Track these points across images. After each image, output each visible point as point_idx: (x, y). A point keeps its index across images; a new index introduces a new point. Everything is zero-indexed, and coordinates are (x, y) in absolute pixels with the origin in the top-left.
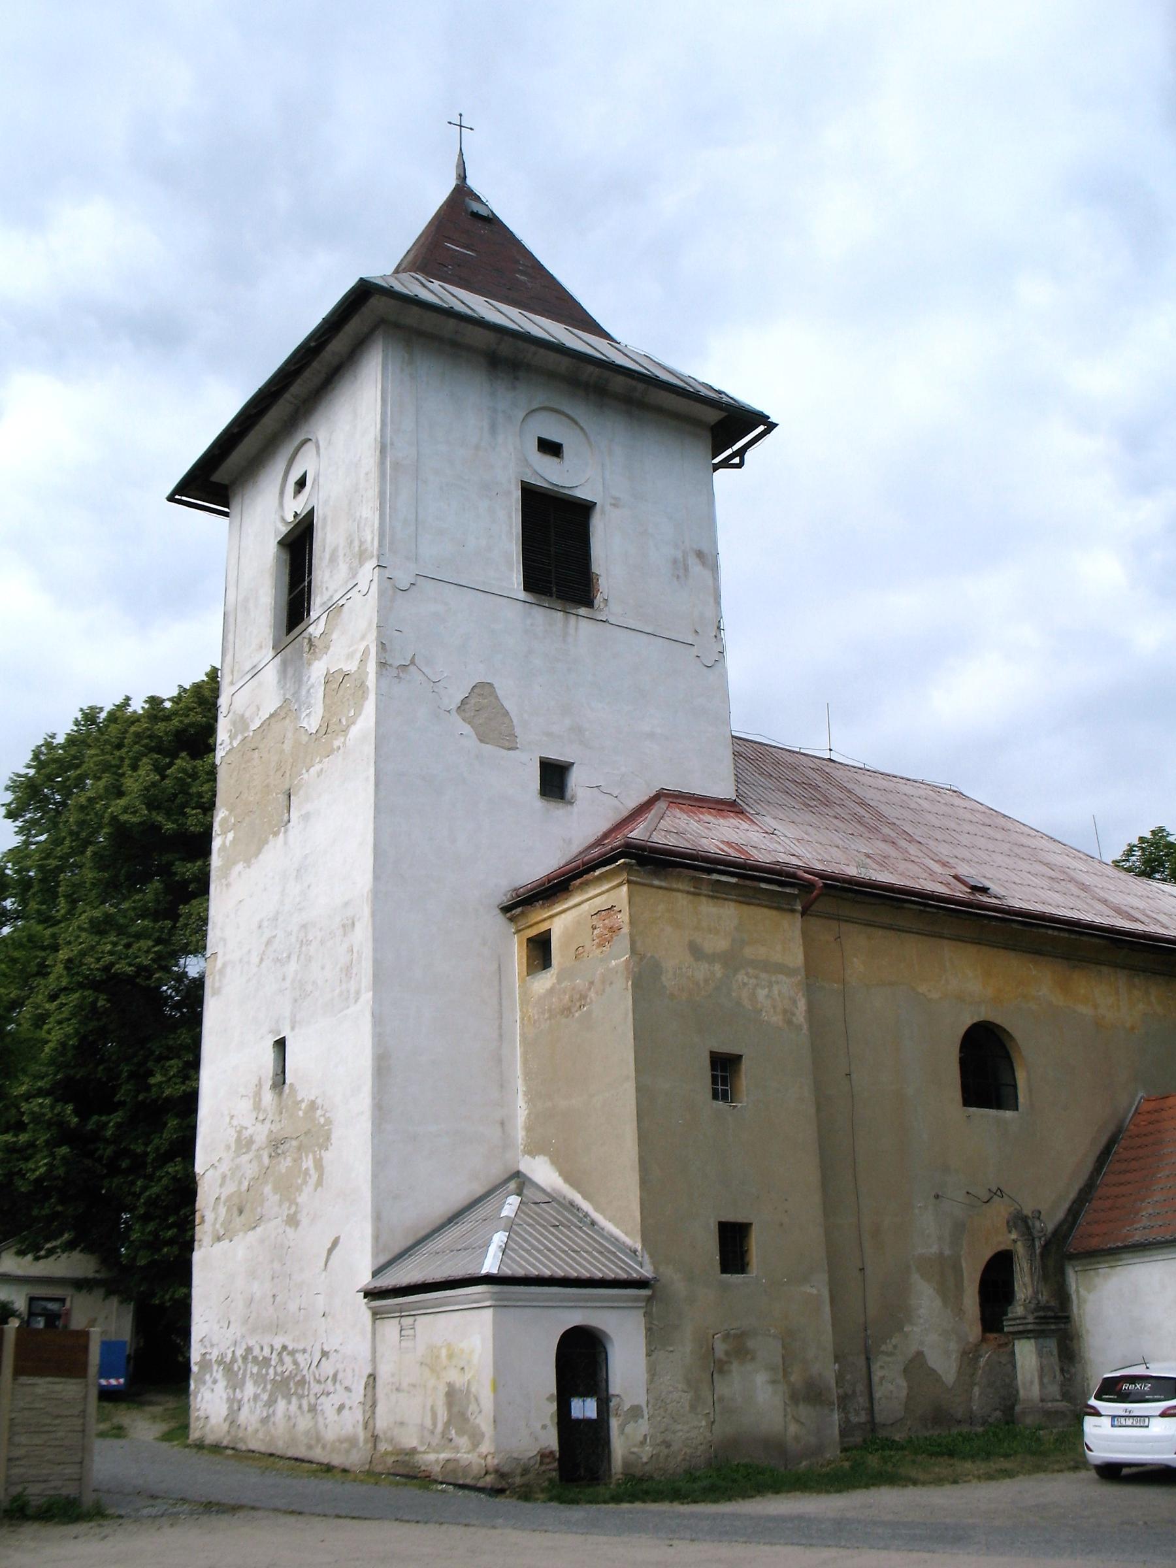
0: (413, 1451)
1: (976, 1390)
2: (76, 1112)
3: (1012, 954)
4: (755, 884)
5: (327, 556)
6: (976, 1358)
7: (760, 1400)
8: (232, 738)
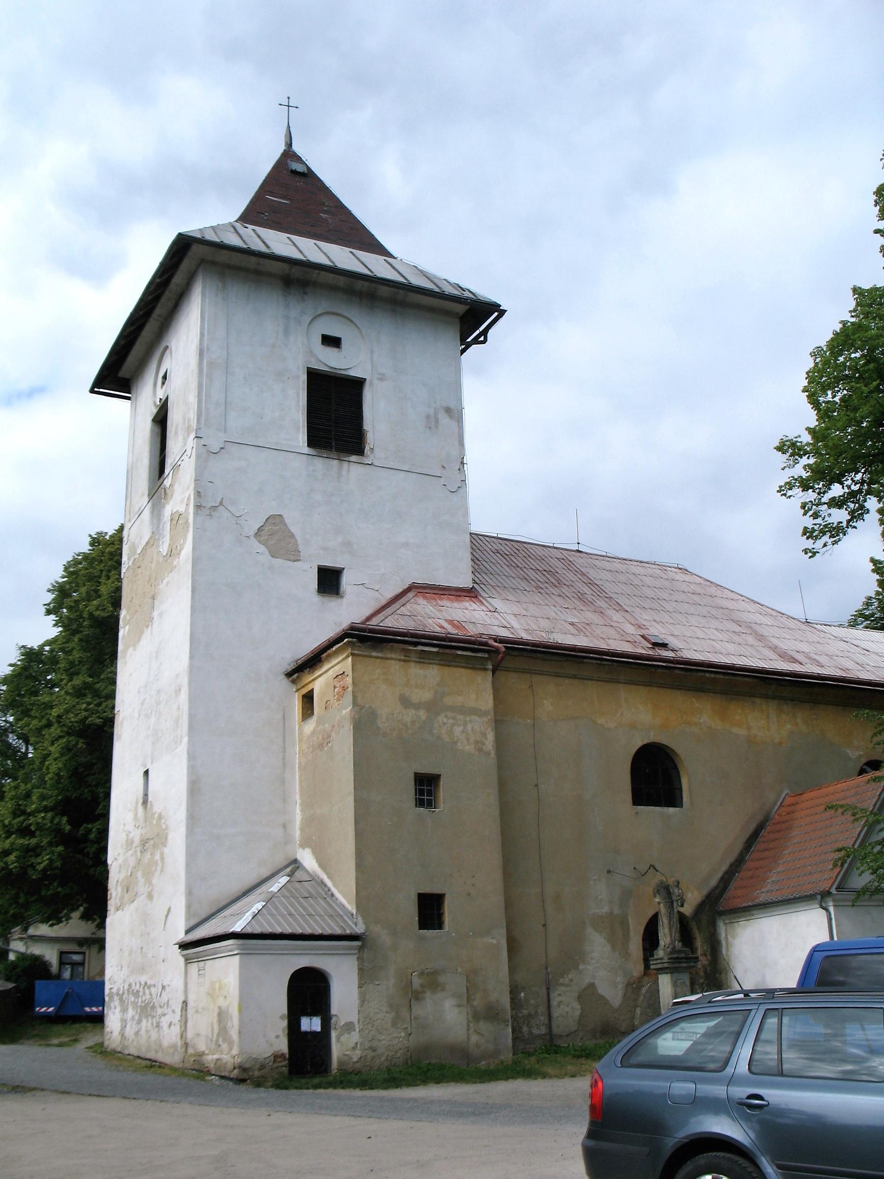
0: (203, 1054)
1: (638, 1011)
2: (69, 822)
3: (678, 692)
4: (453, 651)
5: (174, 429)
6: (639, 988)
7: (448, 1018)
8: (129, 559)
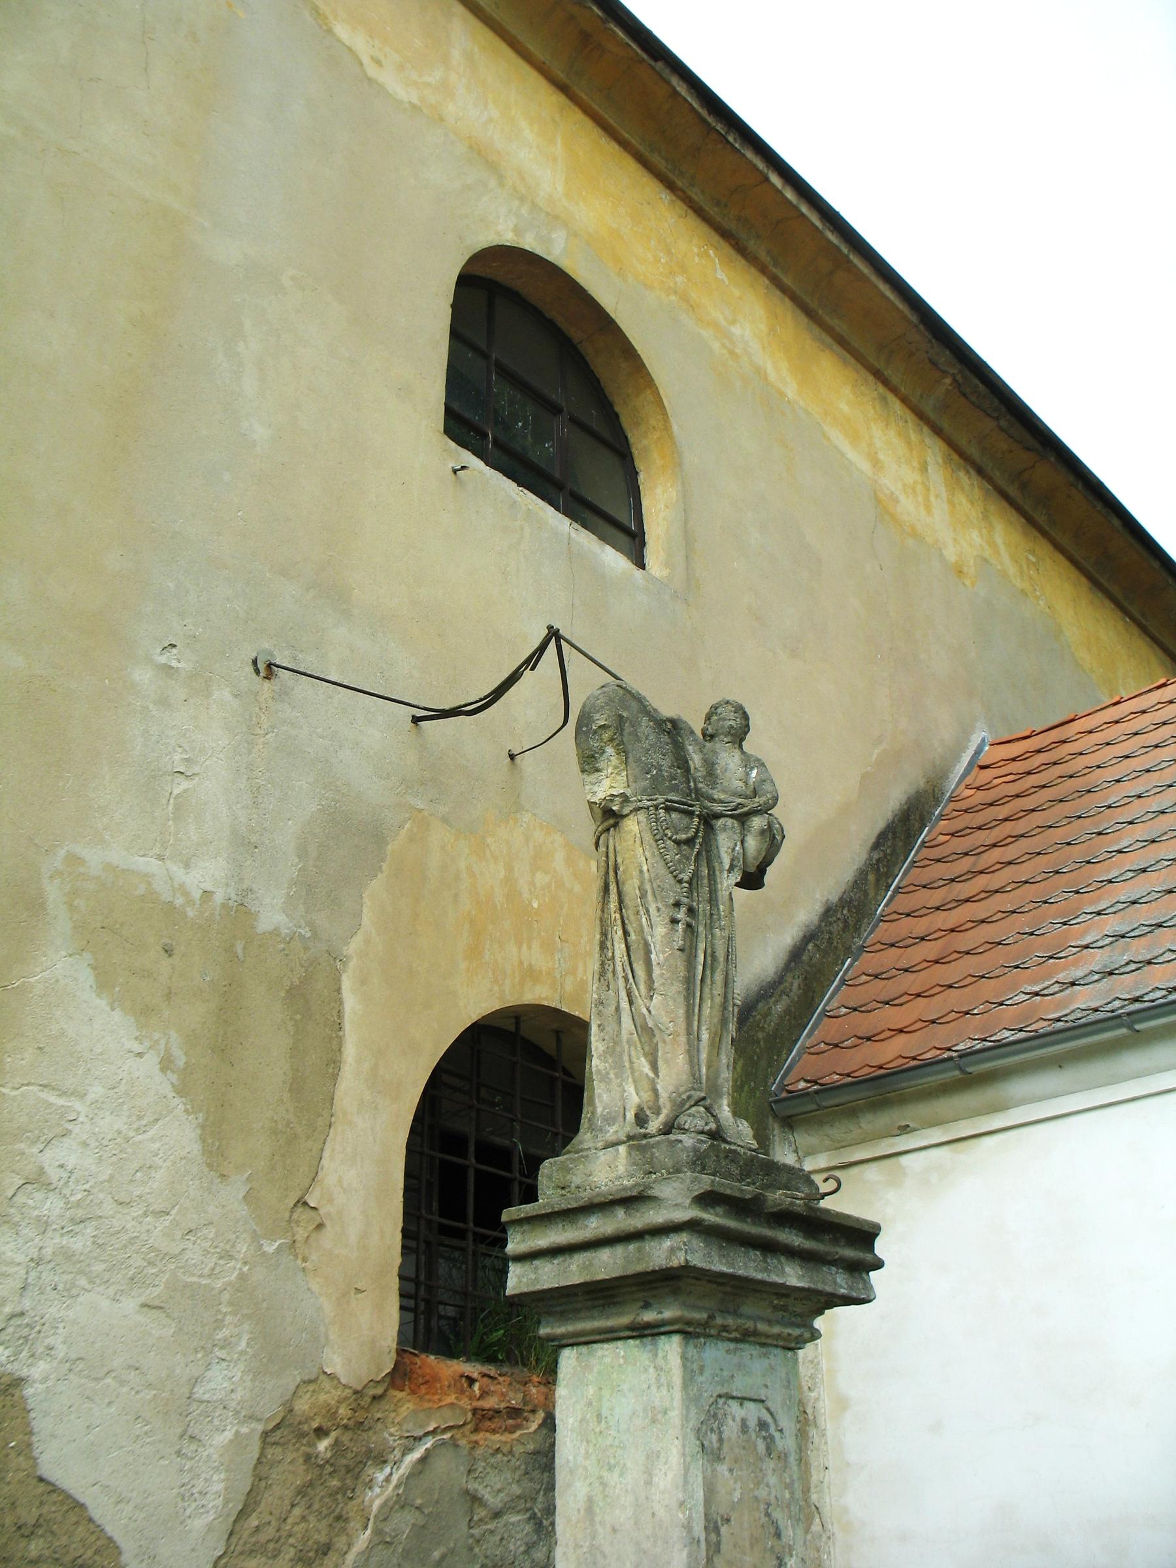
6: (351, 1468)
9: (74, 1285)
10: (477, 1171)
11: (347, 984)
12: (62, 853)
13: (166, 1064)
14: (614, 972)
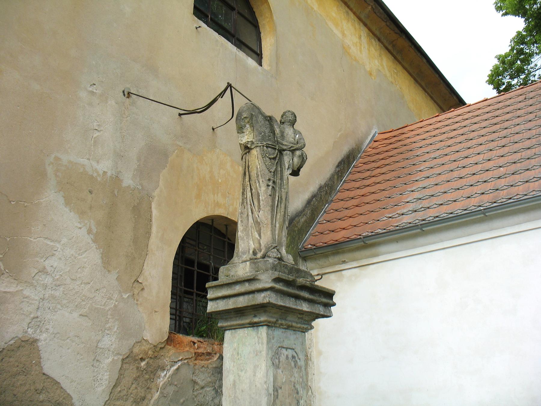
6: (153, 372)
9: (56, 307)
10: (197, 272)
11: (153, 206)
12: (53, 156)
13: (89, 232)
14: (247, 203)
